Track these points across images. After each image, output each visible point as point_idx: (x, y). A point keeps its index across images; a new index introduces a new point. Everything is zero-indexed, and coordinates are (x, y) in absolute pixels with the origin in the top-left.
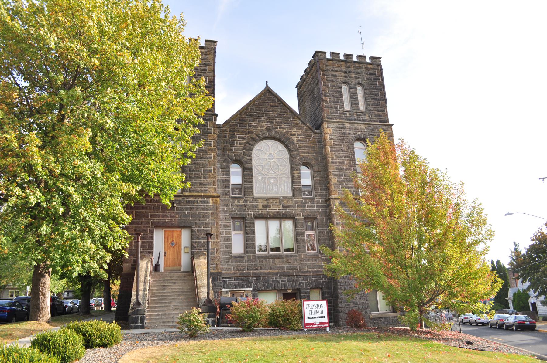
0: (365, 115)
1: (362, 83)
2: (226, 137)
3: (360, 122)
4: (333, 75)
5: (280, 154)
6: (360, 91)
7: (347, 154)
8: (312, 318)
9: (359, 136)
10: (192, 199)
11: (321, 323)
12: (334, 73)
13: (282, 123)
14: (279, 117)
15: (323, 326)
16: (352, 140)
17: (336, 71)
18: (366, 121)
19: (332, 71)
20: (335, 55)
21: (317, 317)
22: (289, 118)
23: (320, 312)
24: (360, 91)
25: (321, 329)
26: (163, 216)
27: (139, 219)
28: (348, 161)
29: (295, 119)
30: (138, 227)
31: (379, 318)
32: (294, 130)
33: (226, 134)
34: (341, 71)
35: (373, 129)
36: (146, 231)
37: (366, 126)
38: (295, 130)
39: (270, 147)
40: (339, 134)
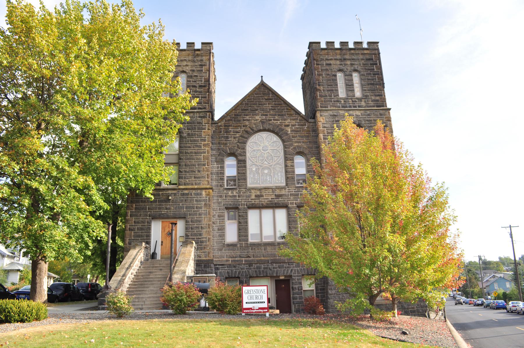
0: (361, 101)
1: (358, 69)
2: (221, 132)
3: (326, 109)
4: (327, 64)
5: (275, 145)
6: (356, 78)
8: (251, 303)
10: (186, 192)
11: (260, 308)
12: (328, 62)
13: (276, 115)
14: (273, 110)
15: (262, 311)
17: (331, 59)
18: (361, 107)
19: (326, 60)
22: (283, 110)
23: (259, 297)
24: (356, 78)
26: (160, 208)
27: (138, 212)
29: (290, 110)
32: (288, 121)
33: (221, 129)
34: (336, 59)
35: (369, 115)
36: (144, 222)
37: (362, 111)
38: (289, 121)
39: (264, 139)
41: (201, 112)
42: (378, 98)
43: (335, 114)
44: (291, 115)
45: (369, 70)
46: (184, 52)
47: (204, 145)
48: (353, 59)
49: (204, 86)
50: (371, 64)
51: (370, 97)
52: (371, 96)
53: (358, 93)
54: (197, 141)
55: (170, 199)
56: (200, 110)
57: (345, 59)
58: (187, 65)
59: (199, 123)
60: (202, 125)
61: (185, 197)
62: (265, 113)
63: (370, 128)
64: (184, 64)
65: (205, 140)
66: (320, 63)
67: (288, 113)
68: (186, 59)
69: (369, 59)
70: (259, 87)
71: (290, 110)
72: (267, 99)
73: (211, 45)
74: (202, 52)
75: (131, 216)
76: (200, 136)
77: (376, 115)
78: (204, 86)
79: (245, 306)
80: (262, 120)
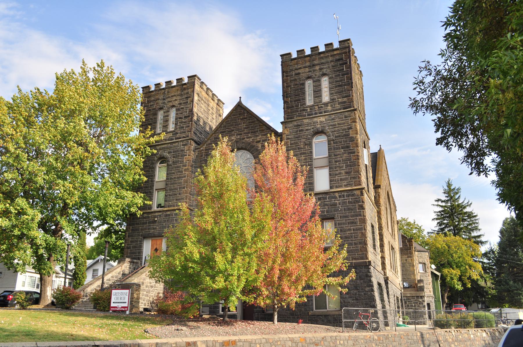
0: (327, 106)
1: (327, 73)
2: (202, 156)
3: (321, 114)
4: (296, 74)
5: (248, 161)
6: (325, 82)
7: (303, 150)
8: (117, 303)
9: (317, 130)
10: (169, 213)
11: (122, 307)
12: (297, 72)
13: (249, 133)
14: (247, 128)
15: (123, 309)
16: (309, 135)
17: (300, 68)
18: (327, 112)
19: (295, 70)
20: (158, 85)
21: (120, 303)
22: (255, 127)
23: (123, 298)
24: (325, 82)
25: (122, 311)
26: (149, 229)
27: (134, 233)
28: (303, 158)
29: (262, 126)
30: (133, 239)
31: (319, 315)
32: (259, 137)
33: (202, 153)
34: (305, 67)
35: (333, 119)
36: (137, 241)
37: (326, 117)
38: (260, 137)
39: (239, 157)
40: (296, 132)
41: (184, 140)
42: (345, 99)
43: (299, 123)
44: (263, 130)
45: (338, 71)
46: (174, 89)
47: (185, 170)
48: (322, 64)
49: (188, 117)
50: (340, 65)
51: (337, 100)
52: (338, 99)
53: (326, 97)
54: (180, 167)
55: (156, 221)
56: (184, 139)
57: (314, 65)
58: (176, 100)
59: (182, 151)
60: (185, 152)
61: (167, 217)
62: (240, 133)
63: (333, 133)
64: (174, 99)
65: (185, 166)
66: (289, 74)
67: (260, 129)
68: (175, 94)
69: (339, 60)
70: (236, 108)
71: (262, 126)
72: (242, 119)
73: (348, 42)
74: (188, 85)
75: (128, 237)
76: (182, 162)
77: (340, 118)
78: (188, 117)
79: (112, 305)
80: (237, 140)
